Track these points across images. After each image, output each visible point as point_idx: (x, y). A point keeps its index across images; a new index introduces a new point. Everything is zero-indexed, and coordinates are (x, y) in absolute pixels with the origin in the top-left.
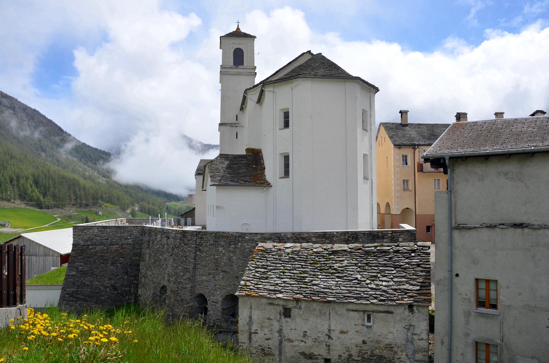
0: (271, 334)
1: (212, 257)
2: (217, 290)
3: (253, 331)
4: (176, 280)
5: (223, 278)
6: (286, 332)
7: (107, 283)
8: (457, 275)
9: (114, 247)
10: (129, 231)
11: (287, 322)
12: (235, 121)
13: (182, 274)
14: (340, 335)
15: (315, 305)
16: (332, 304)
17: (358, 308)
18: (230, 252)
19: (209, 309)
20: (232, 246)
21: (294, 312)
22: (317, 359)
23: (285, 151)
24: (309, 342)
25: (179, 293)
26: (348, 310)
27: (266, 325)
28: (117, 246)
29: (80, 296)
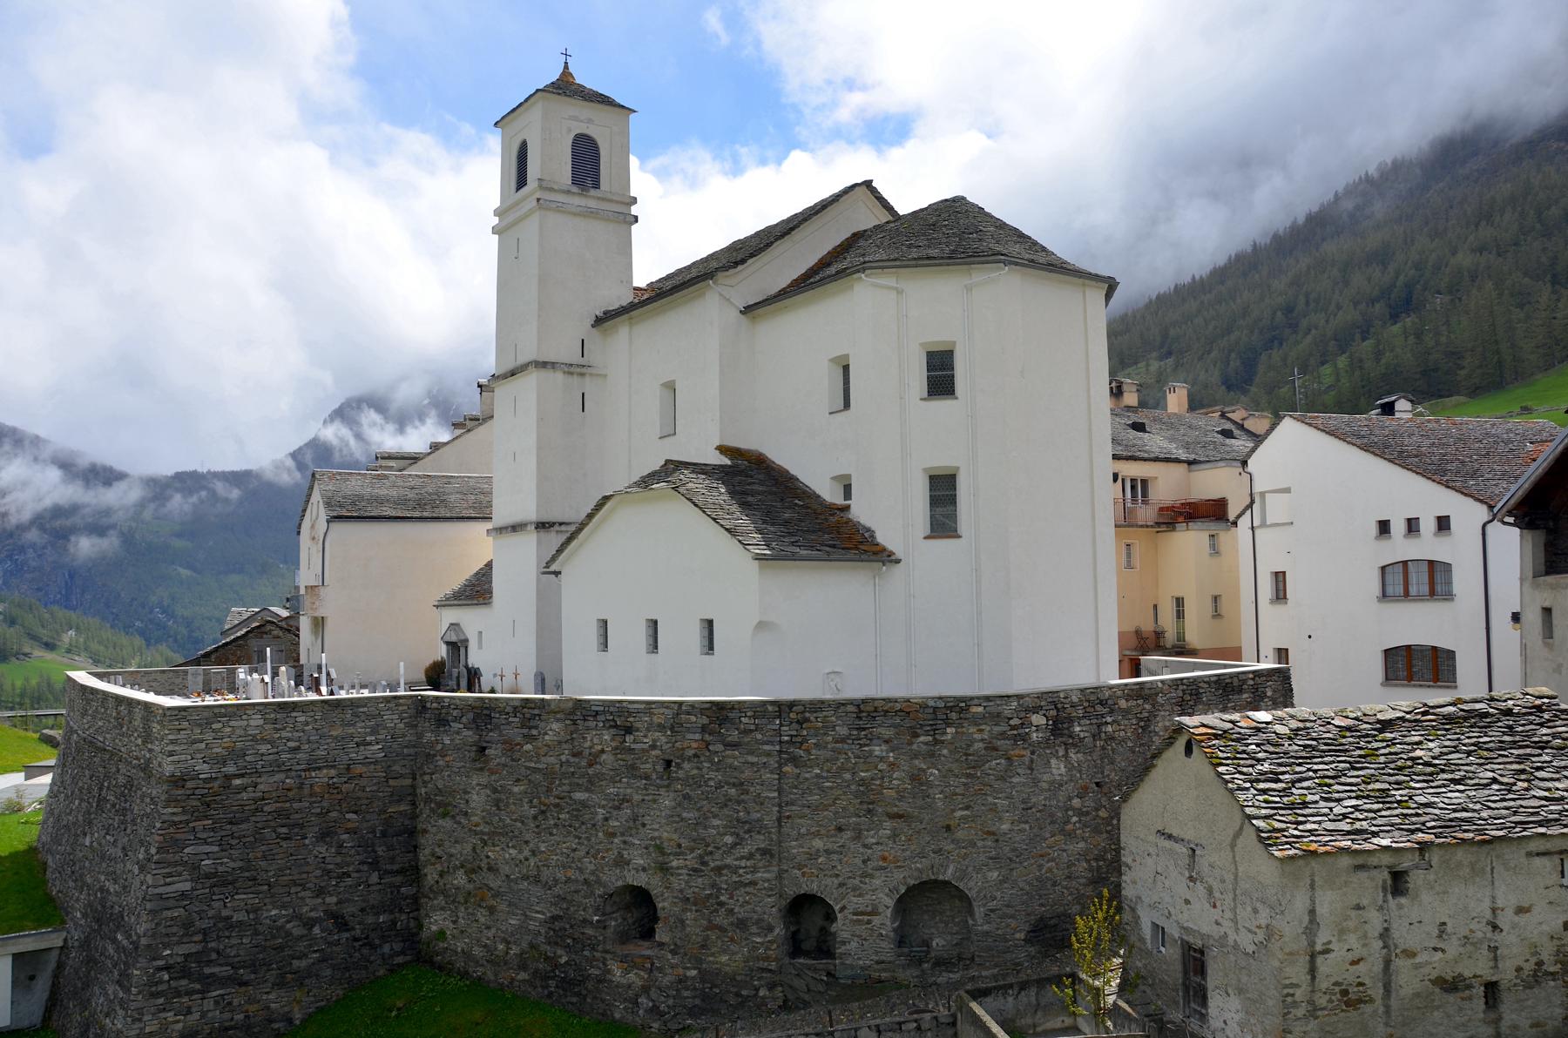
0: (1365, 945)
1: (848, 776)
2: (872, 876)
3: (1319, 948)
4: (704, 863)
5: (894, 836)
6: (1404, 936)
7: (311, 906)
9: (322, 777)
10: (370, 717)
11: (1400, 907)
13: (729, 839)
14: (1516, 919)
15: (1460, 854)
16: (1497, 845)
18: (916, 756)
20: (922, 739)
21: (1416, 879)
22: (1469, 987)
23: (942, 461)
24: (1453, 948)
25: (721, 904)
26: (1529, 854)
27: (1351, 924)
28: (333, 772)
29: (216, 970)
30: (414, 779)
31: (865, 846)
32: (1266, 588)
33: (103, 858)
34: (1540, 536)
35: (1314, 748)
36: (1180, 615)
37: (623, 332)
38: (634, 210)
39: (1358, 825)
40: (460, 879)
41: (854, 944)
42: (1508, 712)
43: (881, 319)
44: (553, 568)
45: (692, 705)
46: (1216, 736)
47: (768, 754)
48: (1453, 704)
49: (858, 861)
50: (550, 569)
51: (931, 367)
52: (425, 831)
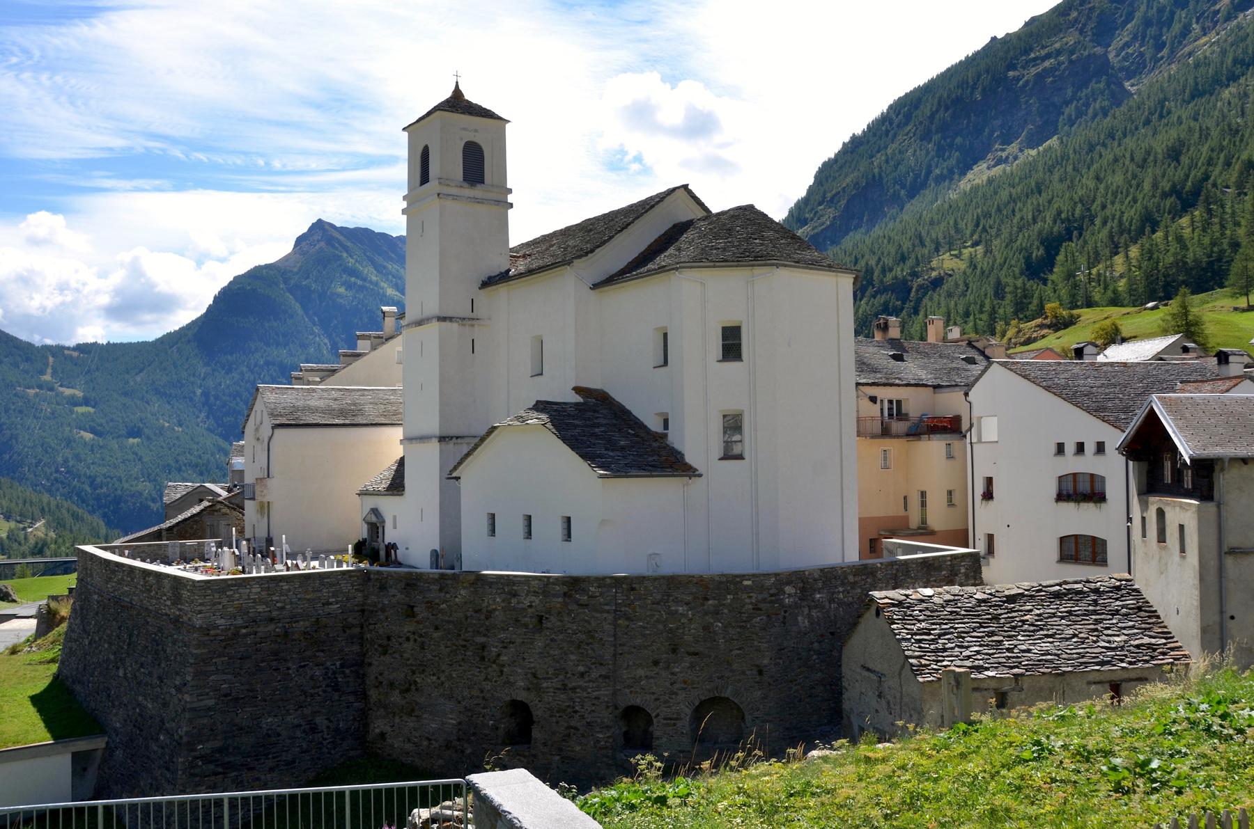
1: (661, 627)
2: (676, 694)
5: (692, 667)
8: (1232, 618)
9: (302, 625)
10: (332, 585)
12: (468, 314)
17: (1102, 678)
18: (706, 614)
19: (657, 733)
21: (1013, 697)
25: (576, 712)
28: (307, 623)
29: (232, 759)
30: (362, 628)
31: (672, 674)
32: (980, 489)
33: (139, 683)
34: (1145, 465)
35: (957, 613)
36: (923, 504)
37: (502, 290)
38: (510, 198)
39: (977, 663)
40: (395, 697)
41: (664, 739)
42: (1096, 591)
43: (696, 299)
44: (454, 475)
45: (557, 579)
46: (893, 605)
47: (608, 612)
48: (1060, 585)
49: (668, 684)
50: (451, 476)
51: (724, 338)
52: (370, 664)
